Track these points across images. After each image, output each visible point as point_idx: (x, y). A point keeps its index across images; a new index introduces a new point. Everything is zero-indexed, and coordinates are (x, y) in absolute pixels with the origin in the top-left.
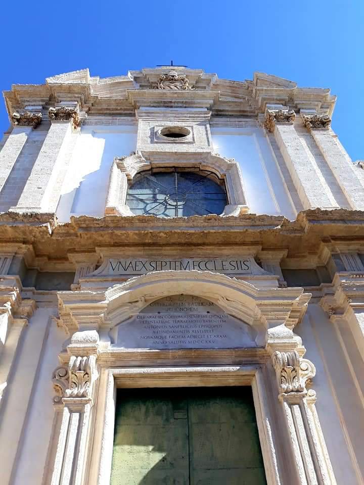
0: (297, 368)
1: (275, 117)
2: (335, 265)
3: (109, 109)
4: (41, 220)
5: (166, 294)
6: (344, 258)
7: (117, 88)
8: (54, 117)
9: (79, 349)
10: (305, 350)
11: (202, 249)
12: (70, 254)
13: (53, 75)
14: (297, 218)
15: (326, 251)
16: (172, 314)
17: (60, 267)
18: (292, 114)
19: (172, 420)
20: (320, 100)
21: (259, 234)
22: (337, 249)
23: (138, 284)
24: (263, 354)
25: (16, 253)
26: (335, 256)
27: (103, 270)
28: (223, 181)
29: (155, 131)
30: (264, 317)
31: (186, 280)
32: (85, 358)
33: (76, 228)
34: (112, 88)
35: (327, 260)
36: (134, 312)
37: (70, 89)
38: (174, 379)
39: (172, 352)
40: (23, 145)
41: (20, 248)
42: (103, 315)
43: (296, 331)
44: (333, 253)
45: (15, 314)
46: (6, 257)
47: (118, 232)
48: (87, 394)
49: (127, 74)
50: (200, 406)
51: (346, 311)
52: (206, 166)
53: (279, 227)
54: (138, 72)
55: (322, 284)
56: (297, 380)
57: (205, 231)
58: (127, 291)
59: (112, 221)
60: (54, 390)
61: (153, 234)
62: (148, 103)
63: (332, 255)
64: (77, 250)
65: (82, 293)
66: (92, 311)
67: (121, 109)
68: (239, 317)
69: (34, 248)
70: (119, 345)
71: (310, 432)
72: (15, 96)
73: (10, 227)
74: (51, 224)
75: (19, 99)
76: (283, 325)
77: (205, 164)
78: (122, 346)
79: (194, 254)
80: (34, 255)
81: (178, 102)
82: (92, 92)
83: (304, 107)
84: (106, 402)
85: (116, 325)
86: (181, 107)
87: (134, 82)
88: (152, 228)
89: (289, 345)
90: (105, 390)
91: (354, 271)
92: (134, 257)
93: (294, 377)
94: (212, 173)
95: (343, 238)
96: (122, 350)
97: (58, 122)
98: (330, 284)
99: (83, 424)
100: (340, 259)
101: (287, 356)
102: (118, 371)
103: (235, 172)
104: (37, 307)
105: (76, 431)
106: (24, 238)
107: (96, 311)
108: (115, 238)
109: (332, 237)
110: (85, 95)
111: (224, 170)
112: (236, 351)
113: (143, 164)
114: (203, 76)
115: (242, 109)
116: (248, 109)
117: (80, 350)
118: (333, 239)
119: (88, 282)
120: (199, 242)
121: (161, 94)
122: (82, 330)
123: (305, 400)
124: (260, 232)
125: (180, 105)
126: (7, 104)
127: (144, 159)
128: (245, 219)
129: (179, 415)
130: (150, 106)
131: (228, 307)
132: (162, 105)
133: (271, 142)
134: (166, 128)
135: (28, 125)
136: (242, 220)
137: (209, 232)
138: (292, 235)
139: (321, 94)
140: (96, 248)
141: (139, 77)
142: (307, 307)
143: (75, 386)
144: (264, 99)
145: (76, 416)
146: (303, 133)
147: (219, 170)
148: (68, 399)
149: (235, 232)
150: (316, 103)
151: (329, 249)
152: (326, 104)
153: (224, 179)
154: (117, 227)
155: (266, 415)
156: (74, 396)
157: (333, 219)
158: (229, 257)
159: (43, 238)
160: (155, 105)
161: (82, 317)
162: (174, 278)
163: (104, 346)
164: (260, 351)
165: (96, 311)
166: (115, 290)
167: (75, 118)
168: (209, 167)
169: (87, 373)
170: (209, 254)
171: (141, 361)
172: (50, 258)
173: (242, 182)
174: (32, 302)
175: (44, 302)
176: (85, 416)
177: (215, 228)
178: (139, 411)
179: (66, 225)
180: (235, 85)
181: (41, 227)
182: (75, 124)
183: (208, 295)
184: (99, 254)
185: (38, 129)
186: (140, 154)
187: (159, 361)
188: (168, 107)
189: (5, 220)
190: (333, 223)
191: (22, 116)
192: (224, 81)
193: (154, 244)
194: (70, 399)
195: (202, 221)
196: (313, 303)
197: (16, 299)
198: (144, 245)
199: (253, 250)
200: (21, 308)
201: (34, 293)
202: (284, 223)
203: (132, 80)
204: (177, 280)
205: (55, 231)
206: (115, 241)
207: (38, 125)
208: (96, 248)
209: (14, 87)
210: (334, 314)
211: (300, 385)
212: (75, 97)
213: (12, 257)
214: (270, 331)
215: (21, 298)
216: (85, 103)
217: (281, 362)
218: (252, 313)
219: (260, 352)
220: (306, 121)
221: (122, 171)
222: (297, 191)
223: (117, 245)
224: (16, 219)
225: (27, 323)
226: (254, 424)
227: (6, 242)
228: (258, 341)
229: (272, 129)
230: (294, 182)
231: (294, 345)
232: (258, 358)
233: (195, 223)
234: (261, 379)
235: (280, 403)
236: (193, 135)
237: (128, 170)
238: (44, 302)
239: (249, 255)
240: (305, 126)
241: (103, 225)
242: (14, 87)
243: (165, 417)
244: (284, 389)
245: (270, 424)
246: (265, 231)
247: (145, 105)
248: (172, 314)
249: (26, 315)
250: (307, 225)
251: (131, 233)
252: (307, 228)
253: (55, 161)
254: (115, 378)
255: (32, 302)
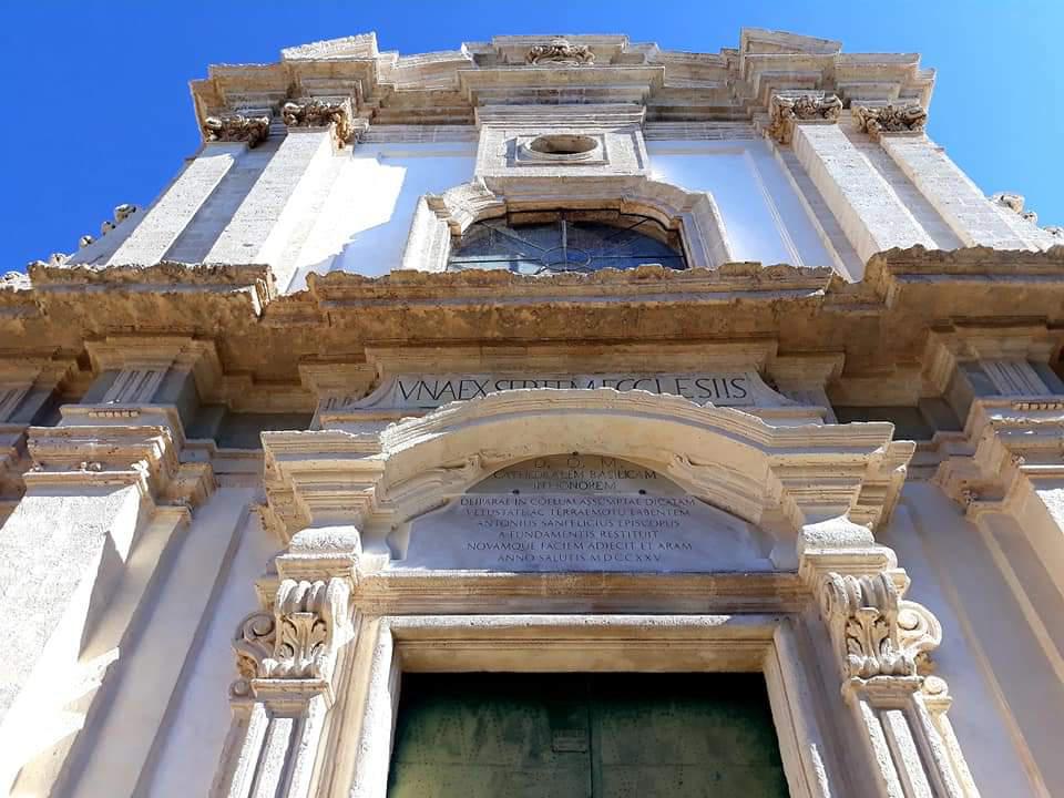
0: (889, 614)
1: (794, 109)
2: (970, 386)
3: (417, 114)
4: (236, 281)
5: (535, 451)
6: (991, 370)
7: (437, 75)
8: (294, 121)
9: (306, 565)
10: (909, 580)
11: (625, 351)
12: (305, 367)
13: (297, 44)
14: (866, 273)
15: (943, 357)
16: (549, 495)
17: (282, 401)
18: (834, 101)
19: (547, 756)
20: (896, 78)
21: (770, 310)
22: (972, 350)
23: (463, 418)
24: (794, 587)
25: (175, 362)
26: (968, 365)
27: (380, 400)
28: (675, 234)
29: (518, 144)
30: (791, 499)
31: (583, 411)
32: (319, 584)
33: (320, 301)
34: (426, 77)
35: (947, 380)
36: (454, 490)
37: (333, 71)
38: (556, 647)
39: (548, 579)
40: (223, 175)
41: (184, 349)
42: (373, 489)
43: (881, 535)
44: (961, 359)
45: (159, 495)
46: (151, 369)
47: (418, 309)
48: (318, 669)
49: (458, 48)
50: (624, 721)
51: (1011, 490)
52: (635, 204)
53: (822, 292)
54: (482, 44)
55: (938, 433)
56: (891, 648)
57: (633, 305)
58: (436, 435)
59: (403, 283)
60: (239, 670)
61: (505, 315)
62: (504, 96)
63: (961, 364)
64: (320, 357)
65: (323, 436)
66: (346, 480)
67: (443, 113)
68: (724, 503)
69: (219, 350)
70: (411, 563)
71: (943, 781)
72: (216, 90)
73: (163, 296)
74: (259, 290)
75: (223, 96)
76: (844, 517)
77: (632, 200)
78: (419, 566)
79: (605, 365)
80: (219, 370)
81: (570, 93)
82: (381, 79)
83: (860, 94)
84: (368, 694)
85: (407, 521)
86: (577, 102)
87: (473, 65)
88: (502, 298)
89: (864, 559)
90: (369, 665)
91: (1023, 394)
92: (457, 371)
93: (883, 641)
94: (650, 218)
95: (984, 321)
96: (420, 571)
97: (302, 131)
98: (959, 434)
99: (302, 746)
100: (983, 372)
101: (861, 586)
102: (402, 621)
103: (705, 211)
104: (216, 486)
105: (282, 763)
106: (196, 327)
107: (357, 480)
108: (410, 324)
109: (958, 320)
110: (366, 83)
111: (678, 209)
112: (716, 579)
113: (488, 202)
114: (626, 47)
115: (716, 105)
116: (729, 103)
117: (308, 569)
118: (959, 324)
119: (342, 421)
120: (618, 335)
121: (530, 76)
122: (317, 525)
123: (919, 697)
124: (773, 306)
125: (574, 98)
126: (198, 109)
127: (491, 193)
128: (732, 275)
129: (569, 742)
130: (508, 103)
131: (694, 482)
132: (534, 98)
133: (787, 162)
134: (543, 139)
135: (240, 139)
136: (725, 278)
137: (643, 308)
138: (855, 314)
139: (901, 66)
140: (366, 350)
141: (485, 55)
142: (905, 475)
143: (289, 651)
144: (765, 80)
145: (284, 726)
146: (862, 145)
147: (666, 211)
148: (268, 681)
149: (709, 306)
150: (889, 86)
151: (951, 351)
152: (910, 89)
153: (677, 231)
154: (415, 298)
155: (811, 736)
156: (282, 674)
157: (959, 270)
158: (695, 370)
159: (240, 324)
160: (517, 99)
161: (320, 493)
162: (552, 406)
163: (373, 563)
164: (785, 580)
165: (357, 480)
166: (405, 431)
167: (340, 125)
168: (643, 205)
169: (322, 621)
170: (644, 364)
171: (467, 600)
172: (256, 380)
173: (727, 241)
174: (204, 467)
175: (236, 474)
176: (307, 725)
177: (657, 297)
178: (457, 730)
179: (297, 296)
180: (698, 62)
181: (235, 295)
182: (342, 137)
183: (640, 454)
184: (375, 367)
185: (261, 149)
186: (482, 181)
187: (514, 602)
188: (547, 102)
189: (152, 280)
190: (958, 279)
191: (226, 123)
192: (674, 55)
193: (506, 342)
194: (271, 681)
195: (625, 282)
196: (917, 478)
197: (163, 456)
198: (482, 342)
199: (757, 354)
200: (176, 483)
201: (212, 454)
202: (831, 285)
203: (471, 59)
204: (563, 411)
205: (270, 310)
206: (411, 334)
207: (261, 140)
208: (366, 350)
209: (213, 70)
210: (976, 500)
211: (903, 658)
212: (343, 87)
213: (165, 370)
214: (808, 529)
215: (174, 459)
216: (365, 101)
217: (846, 596)
218: (758, 492)
219: (783, 583)
220: (867, 118)
221: (438, 217)
222: (855, 250)
223: (416, 343)
224: (178, 280)
225: (189, 518)
226: (775, 771)
227: (154, 334)
228: (777, 558)
229: (787, 138)
230: (847, 232)
231: (879, 562)
232: (778, 600)
233: (608, 288)
234: (790, 649)
235: (848, 709)
236: (605, 149)
237: (453, 214)
238: (236, 474)
239: (747, 365)
240: (866, 130)
241: (383, 292)
242: (213, 70)
243: (527, 748)
244: (857, 666)
245: (822, 759)
246: (787, 303)
247: (498, 100)
248: (549, 495)
249: (187, 498)
250: (891, 286)
251: (449, 310)
252: (891, 293)
253: (287, 199)
254: (397, 641)
255: (204, 467)
